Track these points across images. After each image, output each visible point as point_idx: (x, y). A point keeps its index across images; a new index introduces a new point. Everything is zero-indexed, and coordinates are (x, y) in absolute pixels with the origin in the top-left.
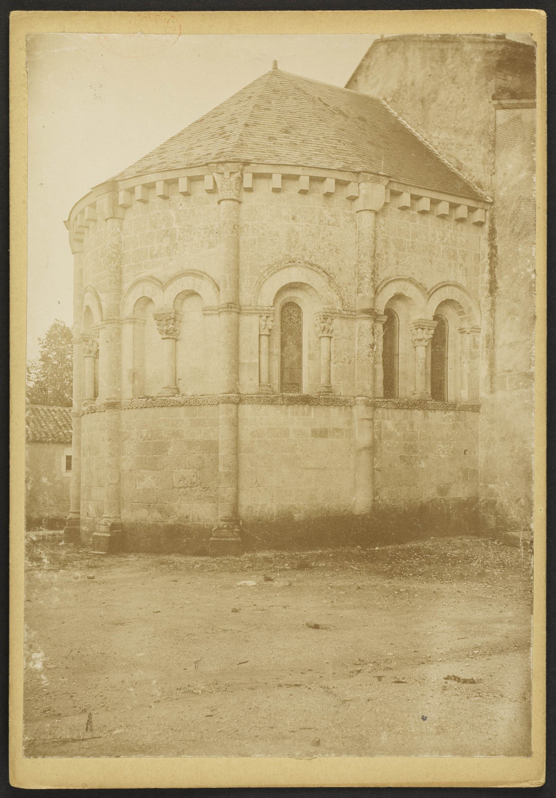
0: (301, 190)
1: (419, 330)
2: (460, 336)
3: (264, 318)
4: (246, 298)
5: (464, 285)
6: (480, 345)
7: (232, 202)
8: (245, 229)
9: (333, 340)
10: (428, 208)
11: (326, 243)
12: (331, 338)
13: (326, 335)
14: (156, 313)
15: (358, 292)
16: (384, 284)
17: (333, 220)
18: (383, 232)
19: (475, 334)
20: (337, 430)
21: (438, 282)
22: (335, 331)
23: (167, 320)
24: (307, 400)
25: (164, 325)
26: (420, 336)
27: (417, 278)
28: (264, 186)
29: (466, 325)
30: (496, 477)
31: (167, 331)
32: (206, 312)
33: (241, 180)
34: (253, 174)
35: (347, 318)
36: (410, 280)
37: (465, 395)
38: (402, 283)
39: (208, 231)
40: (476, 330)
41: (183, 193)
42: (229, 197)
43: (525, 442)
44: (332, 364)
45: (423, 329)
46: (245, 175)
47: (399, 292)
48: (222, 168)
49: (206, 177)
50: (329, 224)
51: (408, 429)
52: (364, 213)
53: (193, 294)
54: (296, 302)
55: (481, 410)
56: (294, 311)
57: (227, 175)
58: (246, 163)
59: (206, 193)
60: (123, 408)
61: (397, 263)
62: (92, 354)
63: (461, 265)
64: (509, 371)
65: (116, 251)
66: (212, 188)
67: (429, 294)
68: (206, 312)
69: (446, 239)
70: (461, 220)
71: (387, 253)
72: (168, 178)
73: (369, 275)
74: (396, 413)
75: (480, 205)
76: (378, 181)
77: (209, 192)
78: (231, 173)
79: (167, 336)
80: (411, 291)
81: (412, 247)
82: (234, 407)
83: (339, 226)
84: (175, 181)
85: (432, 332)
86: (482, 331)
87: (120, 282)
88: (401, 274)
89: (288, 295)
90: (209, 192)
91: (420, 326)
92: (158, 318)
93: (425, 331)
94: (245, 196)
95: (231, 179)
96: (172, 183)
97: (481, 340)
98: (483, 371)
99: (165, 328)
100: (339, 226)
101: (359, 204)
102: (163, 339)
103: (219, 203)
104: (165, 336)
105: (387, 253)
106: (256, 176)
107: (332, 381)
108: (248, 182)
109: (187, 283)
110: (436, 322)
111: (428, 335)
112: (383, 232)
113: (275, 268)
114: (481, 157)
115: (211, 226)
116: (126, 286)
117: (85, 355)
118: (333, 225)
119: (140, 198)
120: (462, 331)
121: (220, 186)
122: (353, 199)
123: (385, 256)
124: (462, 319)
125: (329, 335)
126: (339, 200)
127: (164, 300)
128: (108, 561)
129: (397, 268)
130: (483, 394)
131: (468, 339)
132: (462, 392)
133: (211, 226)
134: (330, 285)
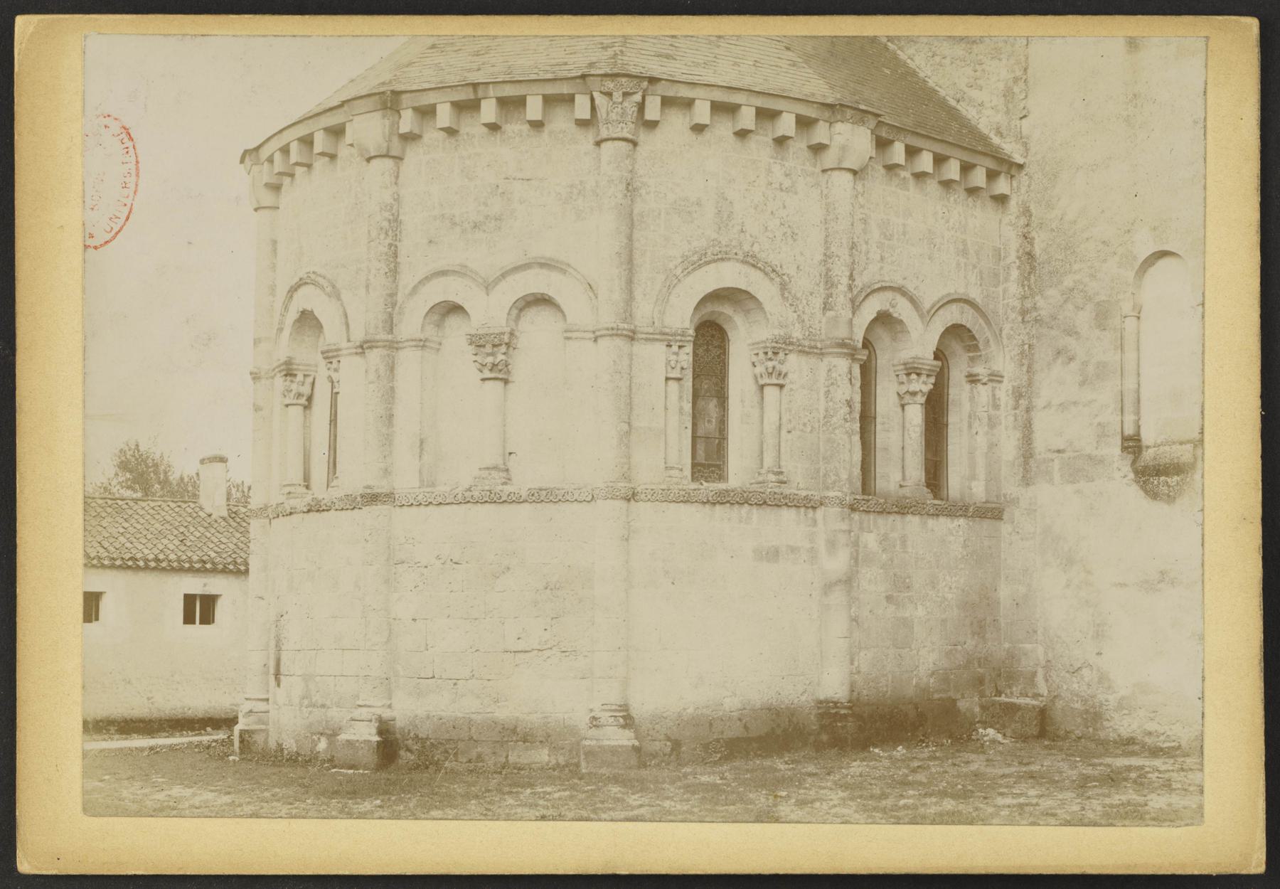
0: (697, 125)
1: (914, 376)
2: (967, 387)
3: (675, 348)
4: (644, 311)
5: (979, 300)
6: (1002, 403)
7: (624, 143)
8: (643, 191)
9: (785, 389)
10: (930, 169)
11: (777, 222)
12: (781, 386)
13: (776, 382)
14: (473, 332)
15: (826, 307)
16: (864, 294)
17: (787, 183)
18: (862, 207)
19: (995, 385)
20: (793, 549)
21: (940, 295)
22: (790, 376)
23: (494, 346)
24: (742, 499)
25: (488, 355)
26: (914, 387)
27: (910, 287)
28: (677, 123)
29: (979, 369)
30: (1035, 632)
31: (494, 365)
32: (569, 335)
33: (641, 107)
34: (713, 102)
35: (808, 353)
36: (901, 291)
37: (979, 491)
38: (889, 295)
39: (575, 191)
40: (996, 378)
41: (487, 125)
42: (620, 135)
43: (1089, 572)
44: (784, 432)
45: (918, 375)
46: (649, 99)
47: (884, 308)
48: (610, 85)
49: (577, 97)
50: (781, 190)
51: (898, 548)
52: (836, 173)
53: (542, 300)
54: (720, 321)
55: (1005, 517)
56: (713, 336)
57: (617, 96)
58: (653, 80)
59: (573, 125)
60: (397, 503)
61: (882, 259)
62: (303, 401)
63: (975, 267)
64: (1059, 451)
65: (387, 214)
66: (588, 117)
67: (927, 316)
68: (569, 335)
69: (952, 221)
70: (973, 191)
71: (867, 243)
72: (505, 94)
73: (845, 281)
74: (881, 520)
75: (1005, 168)
76: (862, 122)
77: (582, 123)
78: (626, 94)
79: (493, 375)
80: (903, 310)
81: (904, 234)
82: (623, 504)
83: (796, 193)
84: (520, 102)
85: (932, 380)
86: (1005, 380)
87: (394, 272)
88: (887, 278)
89: (710, 308)
90: (582, 123)
91: (912, 370)
92: (477, 342)
93: (924, 378)
94: (643, 136)
95: (626, 104)
96: (768, 116)
97: (1004, 393)
98: (1009, 446)
99: (490, 360)
100: (796, 193)
101: (829, 159)
102: (483, 380)
103: (598, 144)
104: (488, 374)
105: (867, 243)
106: (667, 102)
107: (783, 463)
108: (653, 112)
109: (534, 282)
110: (939, 363)
111: (923, 385)
112: (862, 207)
113: (700, 261)
114: (1001, 86)
115: (581, 182)
116: (407, 279)
117: (288, 401)
118: (787, 190)
119: (447, 125)
120: (973, 379)
121: (604, 116)
122: (818, 149)
123: (864, 247)
124: (972, 359)
125: (781, 382)
126: (799, 146)
127: (488, 311)
128: (117, 736)
129: (881, 268)
130: (1011, 488)
131: (983, 392)
132: (974, 484)
133: (581, 182)
134: (783, 295)
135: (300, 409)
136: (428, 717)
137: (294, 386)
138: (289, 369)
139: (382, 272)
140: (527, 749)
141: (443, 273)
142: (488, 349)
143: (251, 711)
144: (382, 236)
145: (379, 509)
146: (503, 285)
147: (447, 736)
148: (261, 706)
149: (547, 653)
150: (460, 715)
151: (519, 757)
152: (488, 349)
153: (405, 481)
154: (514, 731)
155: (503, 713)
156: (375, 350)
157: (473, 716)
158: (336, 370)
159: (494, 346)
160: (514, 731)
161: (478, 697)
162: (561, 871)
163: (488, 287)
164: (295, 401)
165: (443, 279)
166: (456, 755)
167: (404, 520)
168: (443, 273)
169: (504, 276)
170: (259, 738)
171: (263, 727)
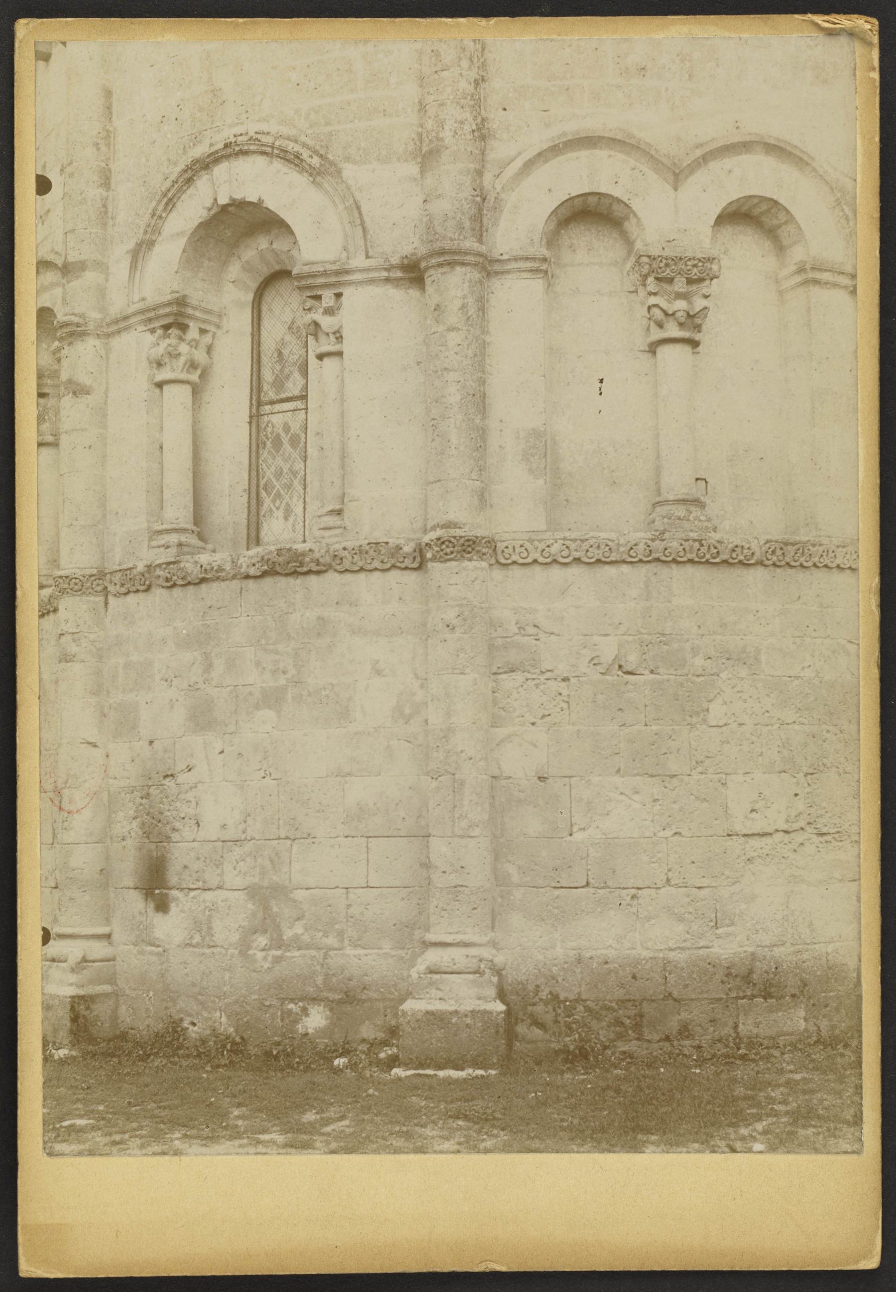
25: (679, 296)
109: (755, 177)
135: (186, 390)
136: (579, 960)
137: (184, 348)
138: (181, 314)
139: (467, 128)
140: (771, 1010)
141: (588, 141)
142: (680, 285)
143: (84, 960)
144: (465, 64)
145: (473, 567)
146: (700, 177)
147: (619, 994)
148: (98, 949)
149: (799, 838)
150: (645, 954)
151: (757, 1025)
152: (680, 285)
153: (516, 516)
154: (747, 978)
155: (728, 947)
156: (458, 269)
157: (671, 955)
158: (329, 311)
159: (690, 281)
160: (747, 978)
161: (681, 919)
162: (20, 1112)
163: (677, 175)
164: (183, 376)
165: (584, 154)
166: (638, 1027)
167: (519, 595)
168: (588, 141)
169: (705, 159)
170: (101, 1010)
171: (107, 988)
